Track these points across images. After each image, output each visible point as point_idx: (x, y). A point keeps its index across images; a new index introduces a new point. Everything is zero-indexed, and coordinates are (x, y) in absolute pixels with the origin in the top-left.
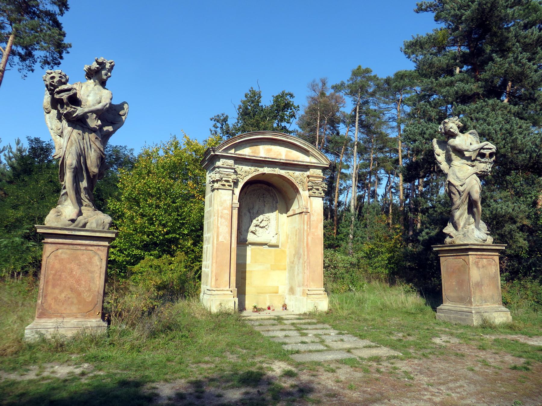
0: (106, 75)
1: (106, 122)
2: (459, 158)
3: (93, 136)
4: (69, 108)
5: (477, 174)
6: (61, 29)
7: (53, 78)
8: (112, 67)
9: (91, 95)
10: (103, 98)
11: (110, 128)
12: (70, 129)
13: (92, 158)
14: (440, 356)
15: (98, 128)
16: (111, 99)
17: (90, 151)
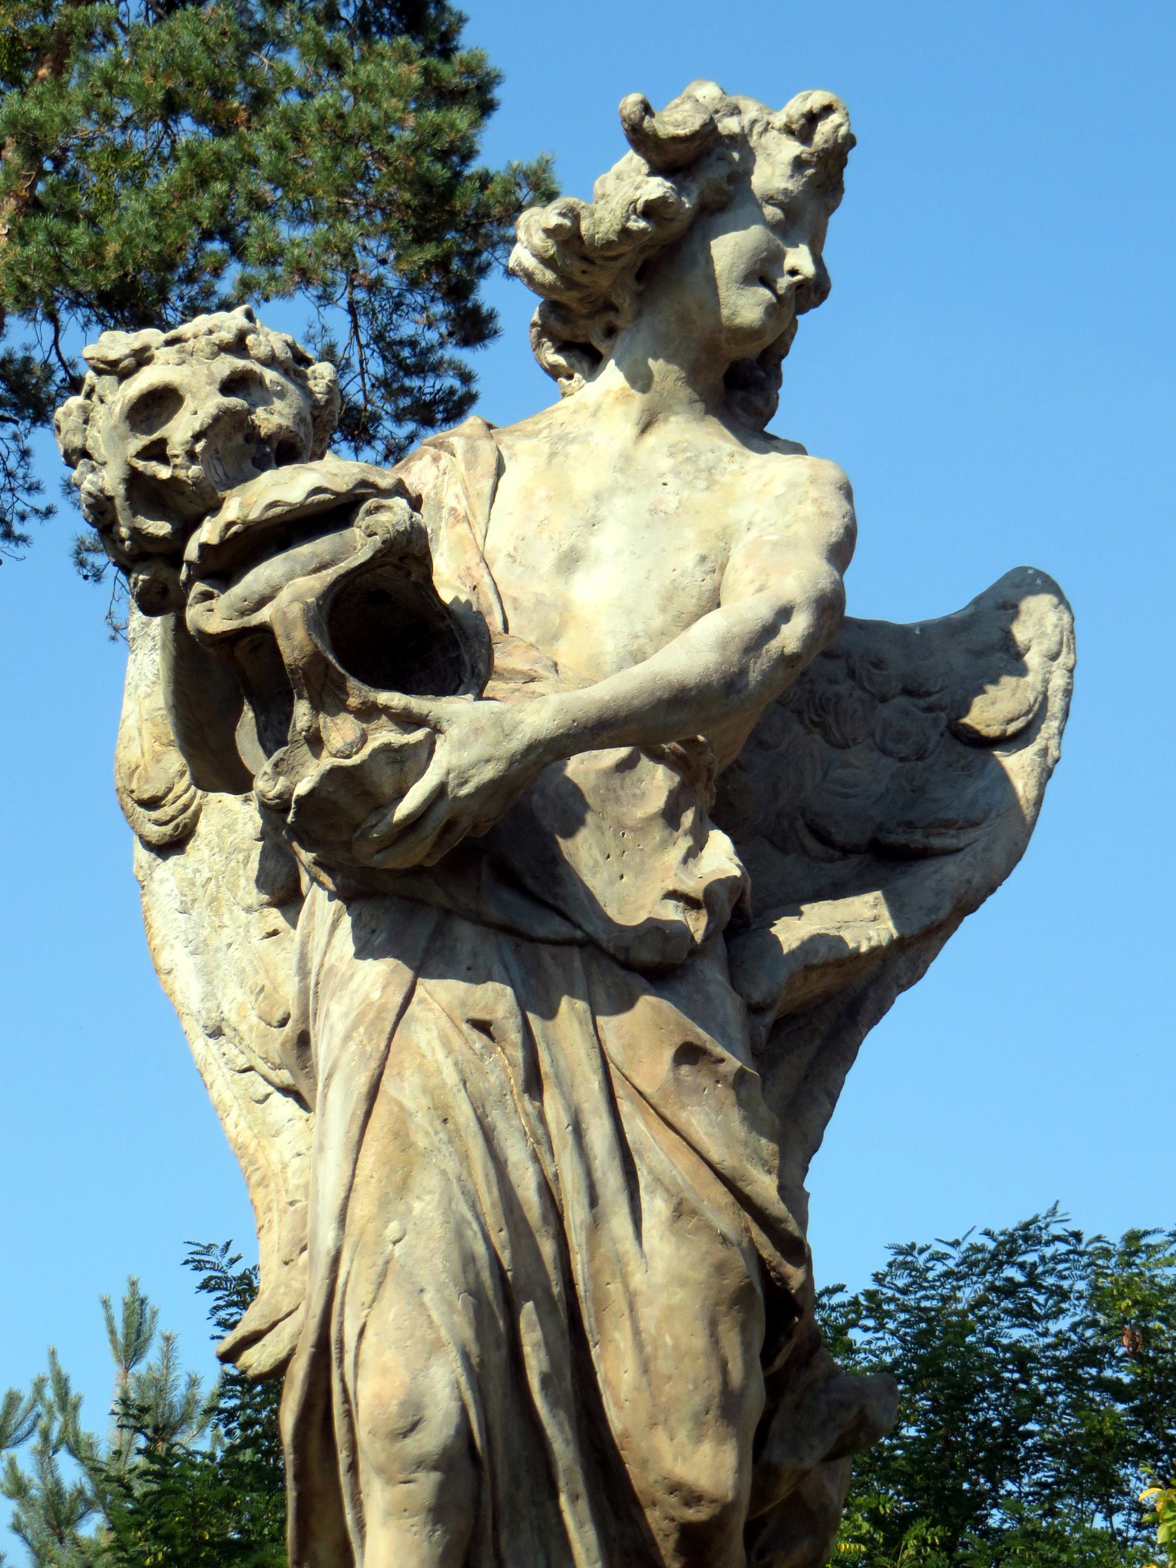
0: (761, 272)
1: (795, 849)
3: (644, 1032)
4: (341, 731)
6: (444, 46)
7: (159, 404)
8: (825, 174)
9: (609, 542)
10: (737, 558)
11: (861, 920)
12: (378, 978)
13: (649, 1316)
14: (1019, 1277)
15: (697, 925)
16: (841, 552)
17: (619, 1222)
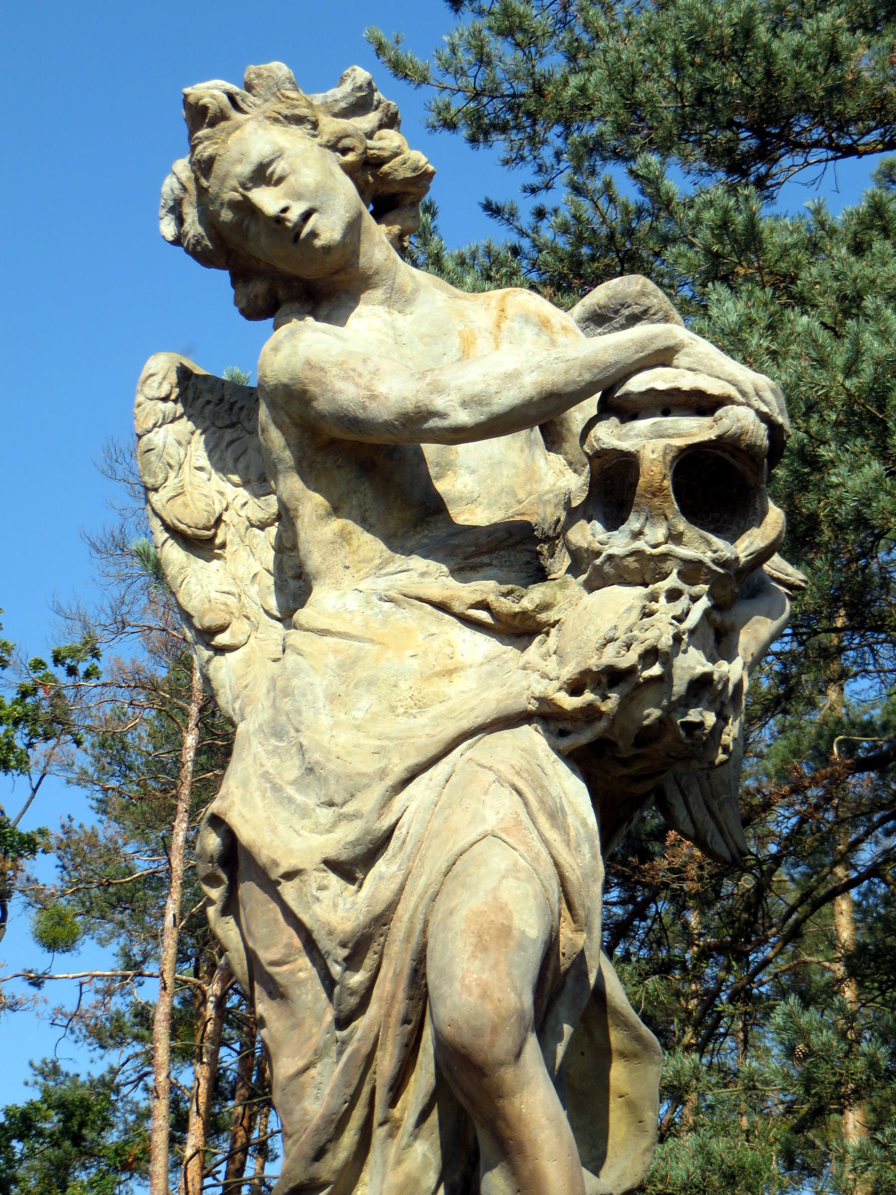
2: (370, 545)
5: (546, 716)
